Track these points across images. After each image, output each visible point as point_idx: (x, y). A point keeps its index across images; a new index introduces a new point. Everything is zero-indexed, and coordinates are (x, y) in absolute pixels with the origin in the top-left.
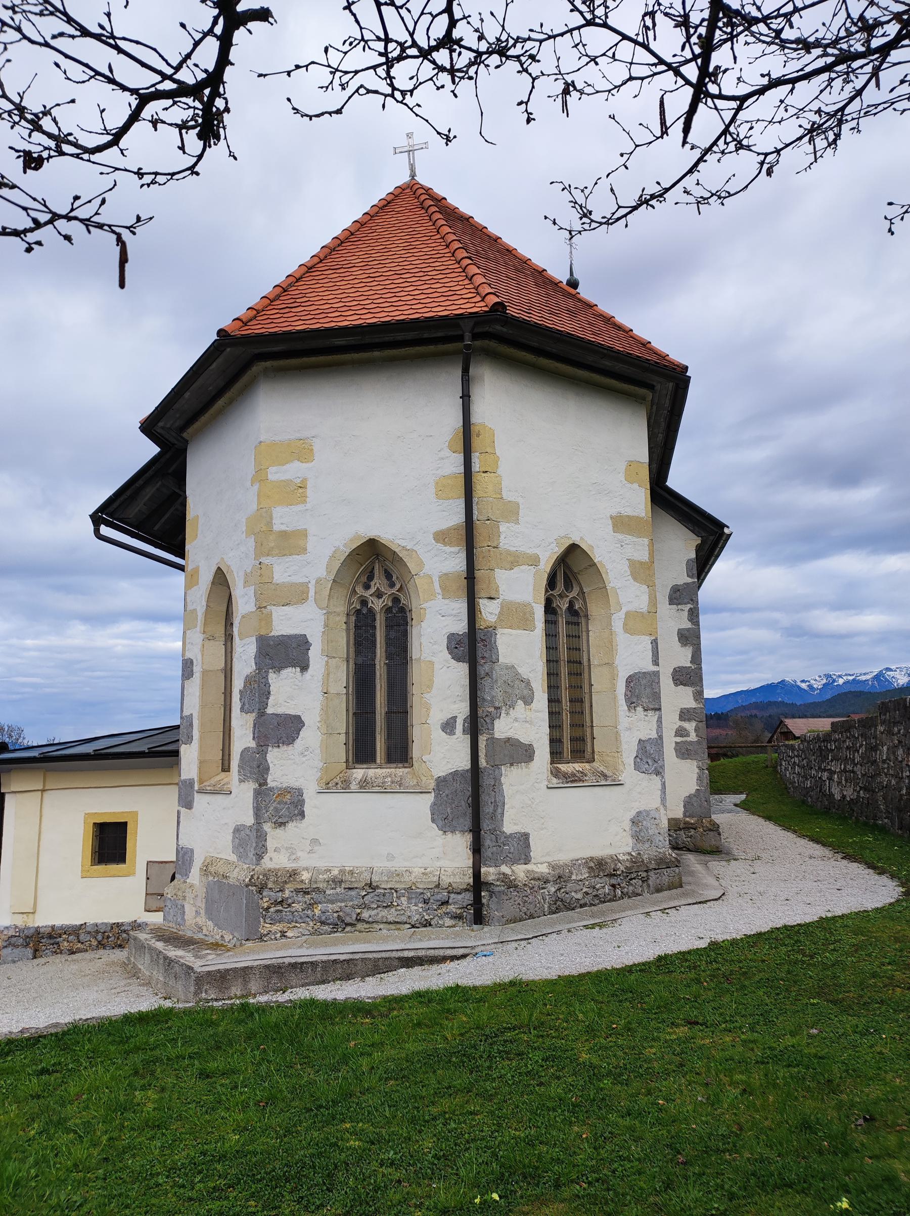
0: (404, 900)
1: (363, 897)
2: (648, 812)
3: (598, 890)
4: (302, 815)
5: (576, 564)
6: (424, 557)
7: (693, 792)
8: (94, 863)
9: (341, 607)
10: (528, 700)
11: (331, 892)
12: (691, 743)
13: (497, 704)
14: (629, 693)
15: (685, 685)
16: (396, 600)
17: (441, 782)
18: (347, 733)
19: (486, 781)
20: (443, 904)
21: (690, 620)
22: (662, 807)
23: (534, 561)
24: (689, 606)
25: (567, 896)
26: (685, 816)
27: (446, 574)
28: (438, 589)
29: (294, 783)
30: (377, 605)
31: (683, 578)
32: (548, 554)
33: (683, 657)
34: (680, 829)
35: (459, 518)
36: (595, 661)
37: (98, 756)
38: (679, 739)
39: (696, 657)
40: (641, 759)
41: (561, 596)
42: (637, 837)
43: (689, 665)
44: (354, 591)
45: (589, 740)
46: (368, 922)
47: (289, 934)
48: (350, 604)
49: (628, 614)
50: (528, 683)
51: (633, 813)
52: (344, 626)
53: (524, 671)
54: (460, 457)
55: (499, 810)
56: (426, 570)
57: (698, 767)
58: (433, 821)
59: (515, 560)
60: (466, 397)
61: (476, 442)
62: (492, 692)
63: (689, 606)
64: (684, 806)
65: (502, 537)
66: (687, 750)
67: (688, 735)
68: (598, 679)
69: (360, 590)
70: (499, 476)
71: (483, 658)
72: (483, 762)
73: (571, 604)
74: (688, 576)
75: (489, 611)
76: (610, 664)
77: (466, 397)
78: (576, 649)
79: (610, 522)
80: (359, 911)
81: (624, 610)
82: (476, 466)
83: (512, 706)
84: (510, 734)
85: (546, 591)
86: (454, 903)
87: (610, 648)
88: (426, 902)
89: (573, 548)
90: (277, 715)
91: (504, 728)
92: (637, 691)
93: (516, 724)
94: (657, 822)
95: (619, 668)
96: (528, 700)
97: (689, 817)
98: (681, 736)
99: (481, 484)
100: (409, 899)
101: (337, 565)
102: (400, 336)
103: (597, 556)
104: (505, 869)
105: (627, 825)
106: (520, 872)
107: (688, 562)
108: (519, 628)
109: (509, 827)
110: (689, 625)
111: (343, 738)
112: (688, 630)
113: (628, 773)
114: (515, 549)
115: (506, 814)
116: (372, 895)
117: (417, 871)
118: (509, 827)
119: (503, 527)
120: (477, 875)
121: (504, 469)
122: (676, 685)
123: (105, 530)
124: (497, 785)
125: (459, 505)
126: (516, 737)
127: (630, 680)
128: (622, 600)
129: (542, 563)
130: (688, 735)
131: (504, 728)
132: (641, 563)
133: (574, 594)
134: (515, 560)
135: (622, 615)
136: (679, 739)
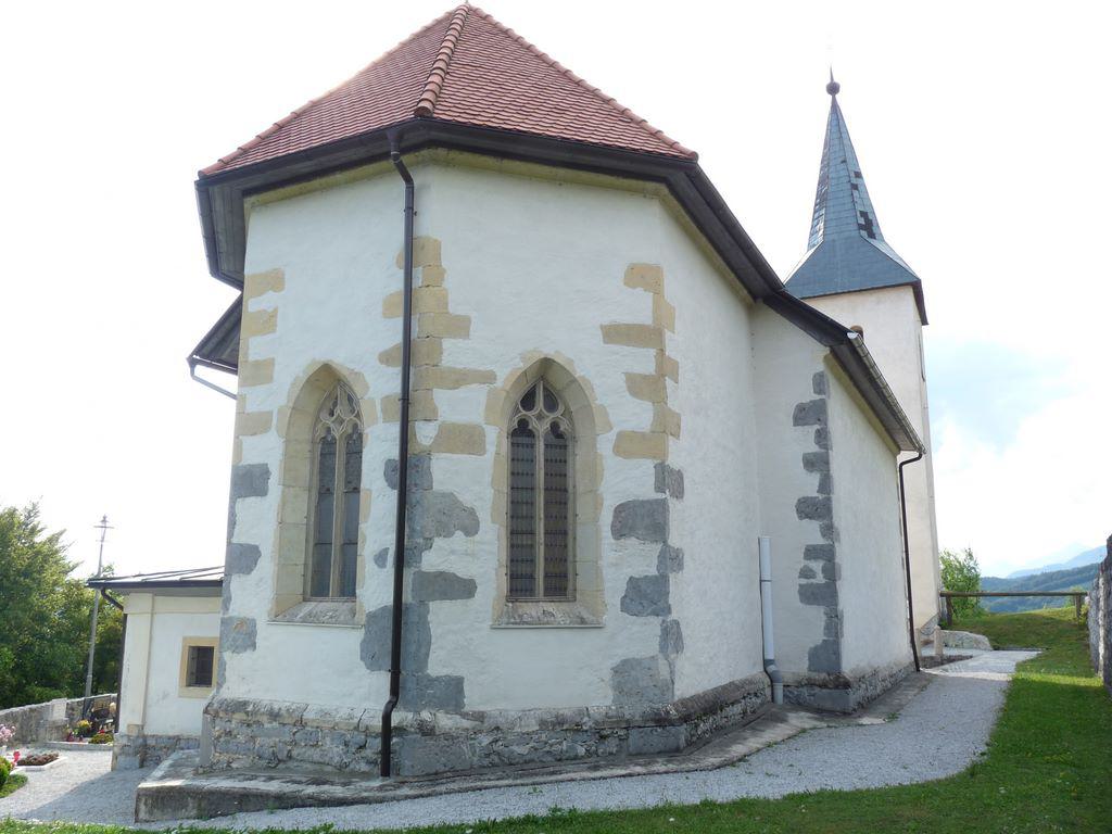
0: (328, 740)
1: (294, 734)
2: (639, 662)
3: (551, 746)
4: (254, 646)
5: (558, 382)
6: (369, 378)
7: (820, 642)
8: (189, 685)
9: (304, 434)
10: (471, 529)
11: (269, 726)
12: (818, 586)
13: (427, 535)
14: (619, 525)
15: (810, 518)
16: (355, 426)
17: (372, 617)
18: (305, 565)
19: (410, 618)
20: (361, 747)
21: (818, 443)
22: (660, 656)
23: (487, 378)
24: (817, 427)
25: (506, 749)
26: (809, 669)
27: (387, 397)
28: (380, 414)
29: (250, 616)
30: (337, 433)
31: (809, 395)
32: (507, 371)
33: (810, 485)
34: (802, 686)
35: (399, 339)
36: (581, 489)
37: (183, 584)
38: (804, 581)
39: (826, 485)
40: (632, 600)
41: (540, 417)
42: (620, 689)
43: (816, 495)
44: (317, 419)
45: (570, 577)
46: (297, 760)
47: (234, 765)
48: (314, 430)
49: (621, 435)
50: (472, 513)
51: (616, 661)
52: (308, 455)
53: (466, 498)
54: (401, 273)
55: (423, 650)
56: (371, 394)
57: (826, 614)
58: (362, 658)
59: (460, 379)
60: (411, 212)
61: (418, 255)
62: (421, 521)
63: (817, 427)
64: (809, 659)
65: (445, 354)
66: (813, 593)
67: (814, 577)
68: (581, 507)
69: (324, 416)
70: (444, 289)
71: (416, 485)
72: (407, 597)
73: (555, 426)
74: (815, 392)
75: (425, 434)
76: (593, 492)
77: (411, 212)
78: (560, 475)
79: (600, 332)
80: (289, 748)
81: (616, 430)
82: (417, 282)
83: (449, 535)
84: (443, 568)
85: (517, 411)
86: (370, 748)
87: (595, 475)
88: (346, 744)
89: (546, 366)
90: (241, 545)
91: (432, 560)
92: (630, 521)
93: (452, 557)
94: (651, 672)
95: (604, 495)
96: (471, 529)
97: (815, 671)
98: (806, 577)
99: (425, 301)
100: (332, 740)
101: (297, 391)
102: (605, 162)
103: (578, 370)
104: (426, 715)
105: (607, 674)
106: (446, 721)
107: (815, 376)
108: (462, 452)
109: (436, 667)
110: (814, 448)
111: (300, 569)
112: (815, 454)
113: (613, 614)
114: (462, 366)
115: (432, 656)
116: (301, 732)
117: (344, 713)
118: (436, 667)
119: (447, 344)
120: (387, 718)
121: (450, 282)
122: (801, 518)
123: (201, 370)
124: (424, 624)
125: (398, 323)
126: (452, 571)
127: (620, 510)
128: (612, 418)
129: (499, 384)
130: (814, 577)
131: (432, 560)
132: (645, 377)
133: (557, 414)
134: (460, 379)
135: (612, 435)
136: (804, 581)
